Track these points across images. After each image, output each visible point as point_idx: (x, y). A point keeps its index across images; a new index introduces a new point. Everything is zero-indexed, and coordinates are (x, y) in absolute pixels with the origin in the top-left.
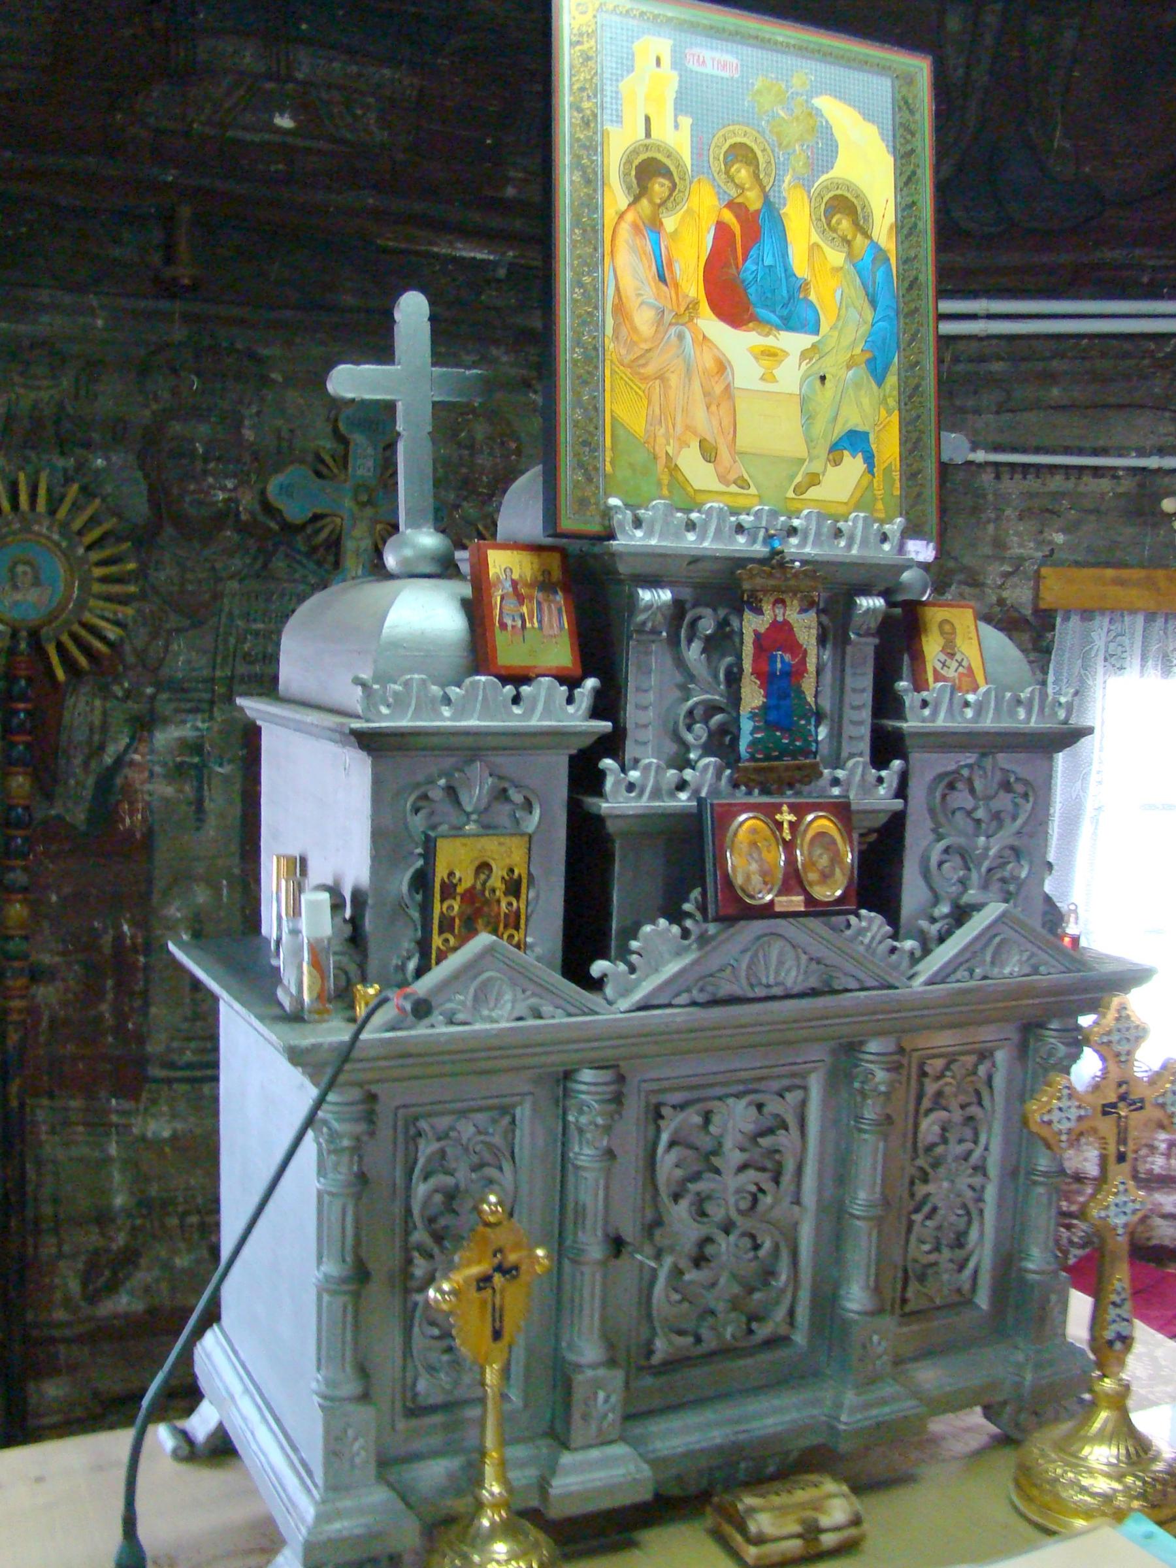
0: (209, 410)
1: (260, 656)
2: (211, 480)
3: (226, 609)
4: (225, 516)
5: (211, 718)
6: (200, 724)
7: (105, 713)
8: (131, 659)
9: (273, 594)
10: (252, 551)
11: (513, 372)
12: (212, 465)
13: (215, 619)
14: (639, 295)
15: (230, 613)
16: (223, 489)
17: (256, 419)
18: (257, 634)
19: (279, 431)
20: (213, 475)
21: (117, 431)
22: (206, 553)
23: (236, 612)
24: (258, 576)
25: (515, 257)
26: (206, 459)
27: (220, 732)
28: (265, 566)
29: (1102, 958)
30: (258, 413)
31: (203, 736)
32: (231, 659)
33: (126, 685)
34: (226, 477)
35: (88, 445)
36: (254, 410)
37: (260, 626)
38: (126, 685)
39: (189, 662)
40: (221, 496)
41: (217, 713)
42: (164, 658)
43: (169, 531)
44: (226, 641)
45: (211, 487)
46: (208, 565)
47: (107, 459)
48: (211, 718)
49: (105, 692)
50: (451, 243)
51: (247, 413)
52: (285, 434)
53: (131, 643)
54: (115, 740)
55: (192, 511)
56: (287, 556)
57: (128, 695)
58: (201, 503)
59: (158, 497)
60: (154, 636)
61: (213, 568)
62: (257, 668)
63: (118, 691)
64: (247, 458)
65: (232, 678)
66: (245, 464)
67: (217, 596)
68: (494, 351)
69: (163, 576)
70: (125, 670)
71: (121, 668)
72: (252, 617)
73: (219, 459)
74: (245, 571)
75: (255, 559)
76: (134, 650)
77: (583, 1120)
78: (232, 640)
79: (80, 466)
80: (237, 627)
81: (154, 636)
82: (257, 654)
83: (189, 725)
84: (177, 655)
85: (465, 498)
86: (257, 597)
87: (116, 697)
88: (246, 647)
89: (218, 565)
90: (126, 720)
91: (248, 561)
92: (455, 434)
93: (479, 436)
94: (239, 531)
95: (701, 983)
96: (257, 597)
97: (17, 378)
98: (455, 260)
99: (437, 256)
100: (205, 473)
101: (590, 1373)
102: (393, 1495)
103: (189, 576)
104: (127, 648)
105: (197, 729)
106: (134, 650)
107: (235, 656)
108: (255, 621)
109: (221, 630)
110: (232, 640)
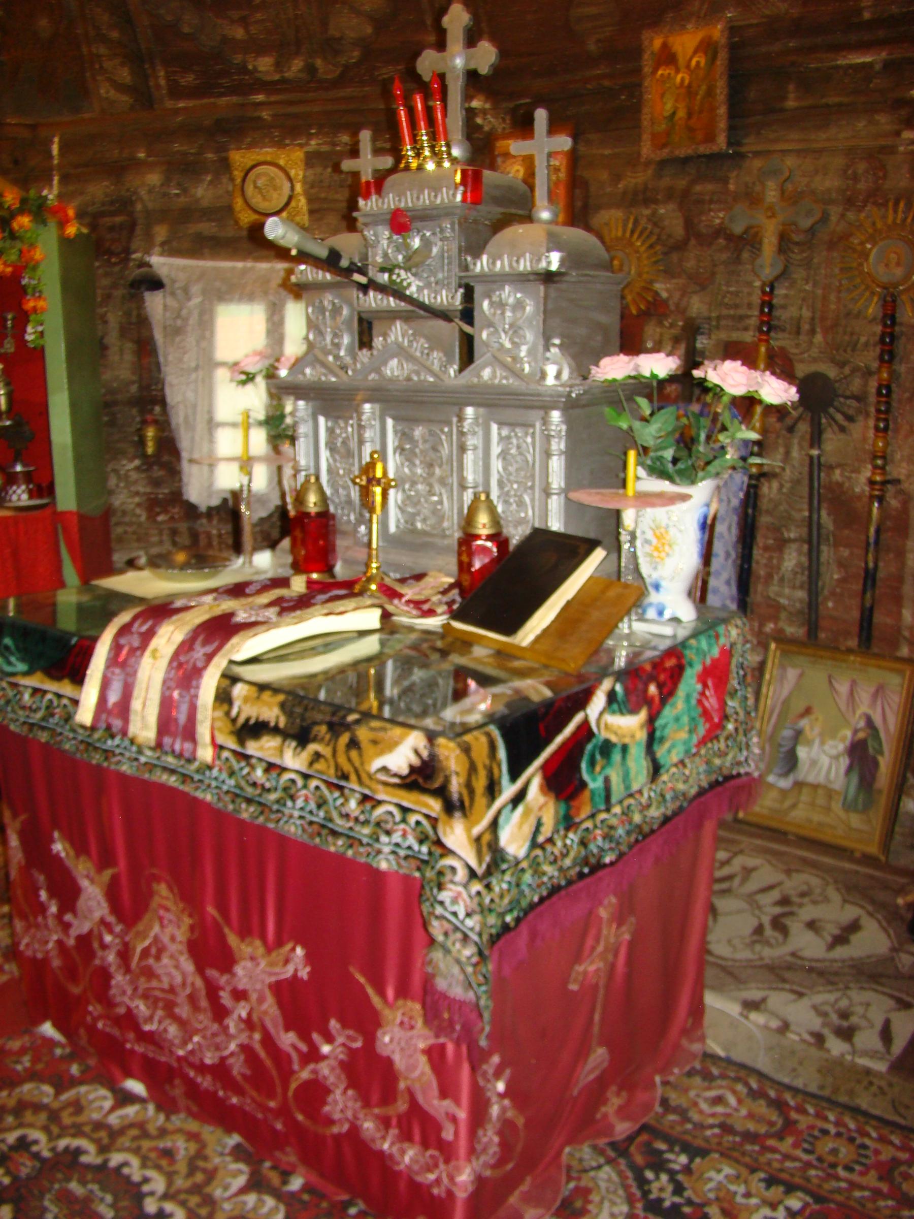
4: (720, 231)
8: (672, 308)
11: (888, 128)
16: (718, 217)
18: (731, 293)
21: (670, 195)
25: (318, 144)
29: (148, 309)
34: (720, 211)
35: (656, 202)
40: (717, 221)
41: (713, 337)
43: (693, 242)
48: (710, 338)
49: (660, 324)
50: (845, 57)
57: (672, 326)
59: (689, 224)
60: (683, 296)
63: (666, 324)
67: (713, 274)
68: (877, 117)
69: (690, 264)
81: (683, 296)
85: (848, 210)
92: (845, 172)
93: (860, 171)
94: (725, 239)
98: (850, 66)
99: (838, 67)
101: (479, 542)
102: (904, 798)
103: (701, 264)
104: (671, 302)
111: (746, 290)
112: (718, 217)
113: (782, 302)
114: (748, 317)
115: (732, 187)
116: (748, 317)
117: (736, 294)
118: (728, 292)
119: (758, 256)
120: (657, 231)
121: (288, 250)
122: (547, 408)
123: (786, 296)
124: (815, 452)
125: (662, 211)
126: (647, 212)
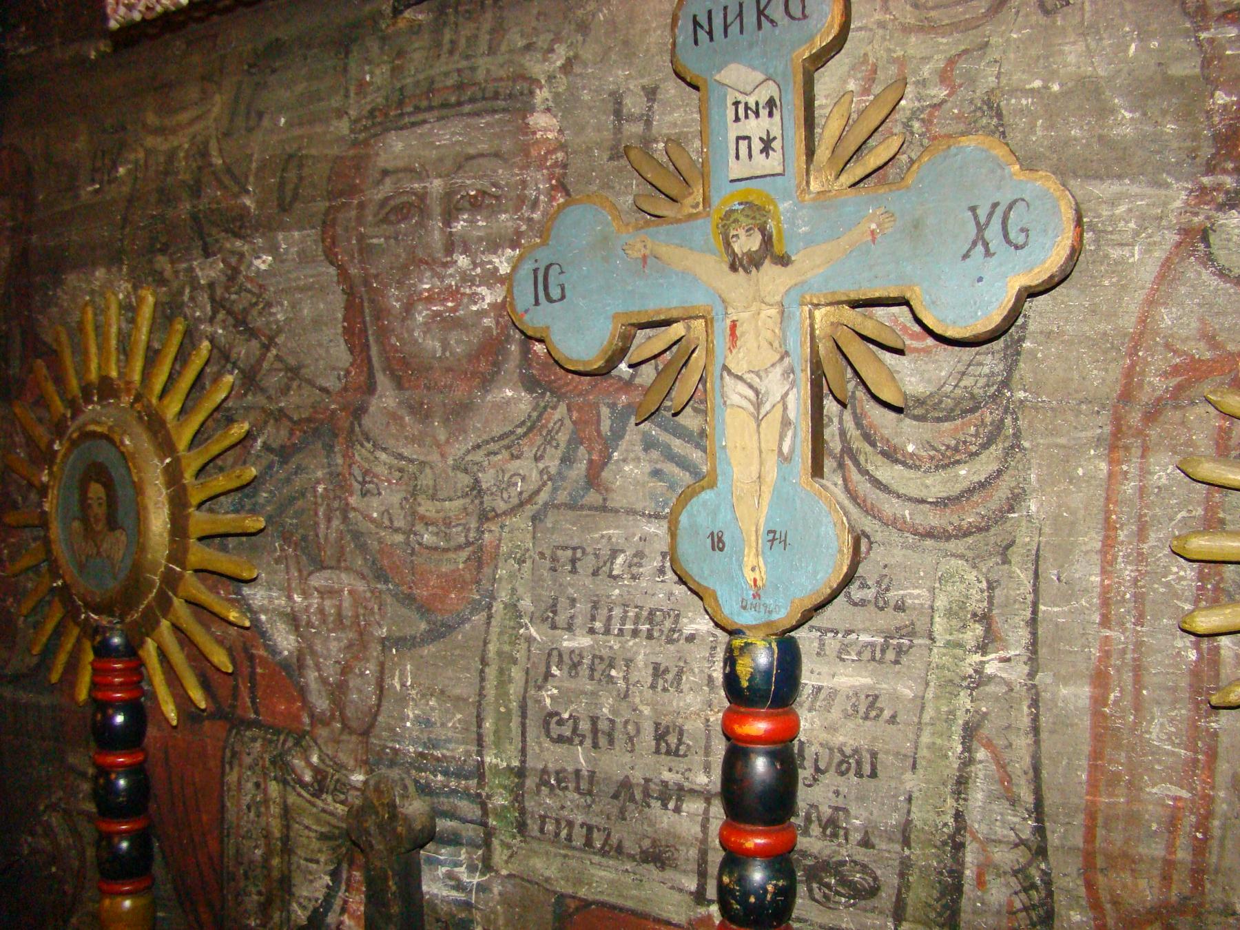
0: (460, 87)
1: (584, 726)
2: (463, 261)
3: (504, 596)
5: (487, 866)
6: (462, 873)
7: (287, 813)
9: (614, 553)
10: (563, 438)
12: (459, 226)
13: (479, 618)
14: (866, 843)
15: (513, 608)
16: (492, 277)
17: (562, 83)
18: (573, 662)
19: (617, 100)
20: (466, 251)
22: (458, 449)
23: (526, 604)
24: (572, 506)
26: (449, 217)
27: (505, 899)
28: (593, 479)
30: (567, 67)
31: (467, 905)
32: (515, 724)
33: (315, 759)
34: (495, 246)
35: (239, 225)
36: (561, 54)
37: (583, 641)
38: (315, 759)
39: (425, 722)
40: (489, 296)
42: (379, 706)
43: (386, 398)
44: (504, 679)
45: (466, 278)
46: (464, 480)
47: (273, 249)
51: (538, 69)
52: (634, 104)
53: (318, 668)
54: (310, 879)
55: (433, 344)
56: (649, 444)
58: (450, 323)
61: (476, 488)
62: (581, 757)
64: (539, 184)
65: (521, 773)
66: (535, 204)
67: (481, 559)
70: (312, 724)
71: (306, 720)
72: (562, 619)
73: (475, 205)
74: (543, 497)
75: (567, 460)
76: (324, 681)
77: (984, 171)
78: (516, 673)
79: (233, 274)
80: (530, 640)
82: (575, 719)
83: (443, 870)
84: (403, 700)
86: (573, 561)
87: (304, 785)
88: (547, 697)
89: (487, 479)
90: (323, 837)
91: (552, 463)
94: (531, 384)
95: (685, 25)
96: (573, 561)
97: (151, 119)
100: (450, 248)
105: (459, 886)
106: (324, 681)
107: (524, 715)
108: (570, 628)
109: (492, 648)
110: (516, 673)
111: (643, 653)
112: (492, 277)
113: (849, 736)
114: (673, 795)
115: (543, 123)
116: (673, 795)
117: (601, 666)
118: (554, 655)
119: (703, 481)
120: (244, 350)
121: (167, 469)
122: (155, 918)
123: (870, 706)
124: (907, 852)
125: (263, 263)
126: (209, 271)
